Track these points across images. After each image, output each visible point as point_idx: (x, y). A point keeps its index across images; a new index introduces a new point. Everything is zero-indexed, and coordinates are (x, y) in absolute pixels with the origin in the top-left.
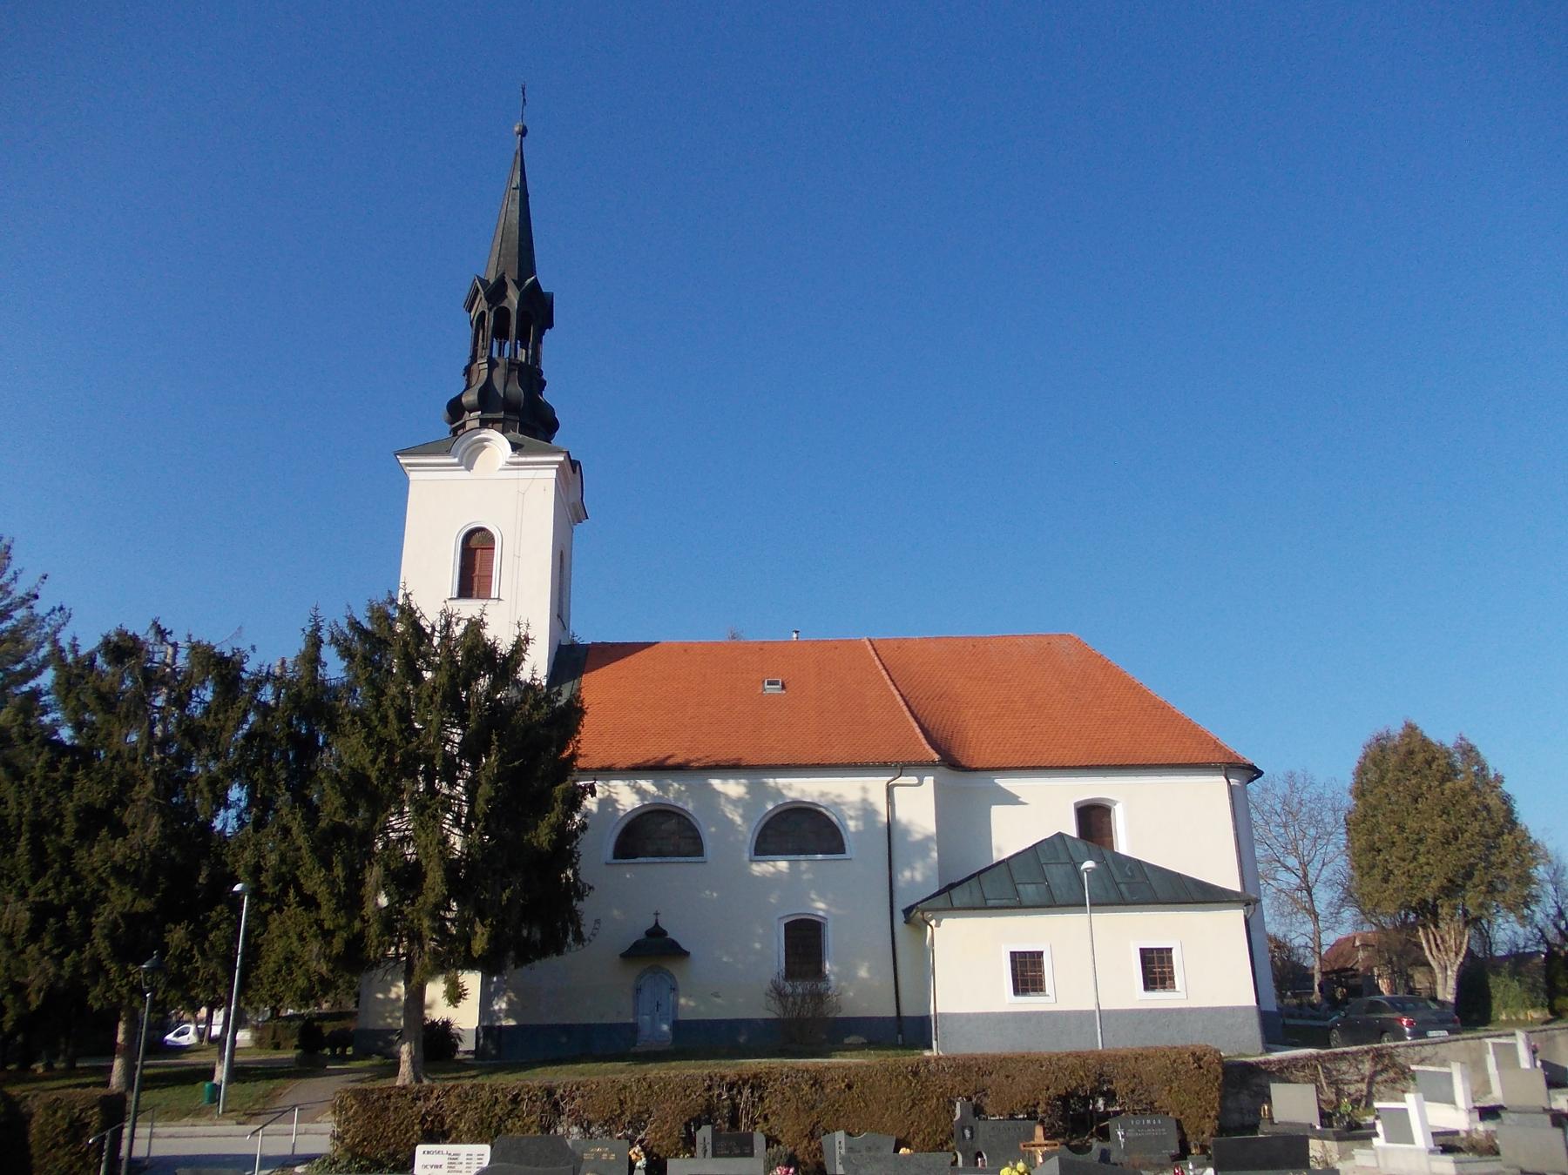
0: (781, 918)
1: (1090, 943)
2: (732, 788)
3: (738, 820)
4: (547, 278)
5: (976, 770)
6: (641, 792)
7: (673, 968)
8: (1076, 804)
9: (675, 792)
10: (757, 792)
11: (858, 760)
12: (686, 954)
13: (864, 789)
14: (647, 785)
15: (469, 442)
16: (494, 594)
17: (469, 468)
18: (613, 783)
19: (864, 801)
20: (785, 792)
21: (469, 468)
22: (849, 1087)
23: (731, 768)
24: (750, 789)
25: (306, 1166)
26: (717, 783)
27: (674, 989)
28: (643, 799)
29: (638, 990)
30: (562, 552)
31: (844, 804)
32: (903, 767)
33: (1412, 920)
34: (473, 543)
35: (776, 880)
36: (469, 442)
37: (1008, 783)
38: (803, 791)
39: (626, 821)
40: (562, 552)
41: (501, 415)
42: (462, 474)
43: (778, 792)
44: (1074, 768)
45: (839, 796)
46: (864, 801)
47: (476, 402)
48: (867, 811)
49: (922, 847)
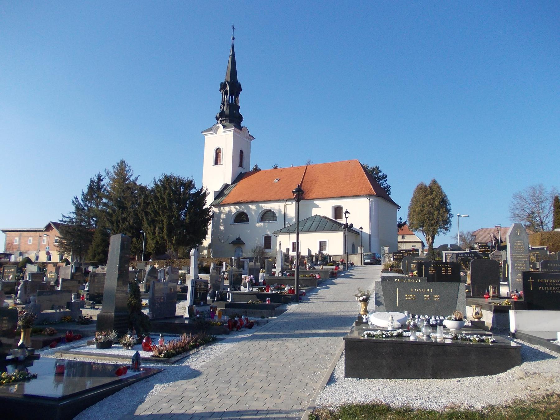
0: (263, 236)
1: (371, 244)
2: (253, 207)
3: (254, 214)
4: (240, 79)
5: (308, 200)
6: (236, 209)
7: (242, 246)
8: (333, 207)
9: (243, 208)
10: (258, 207)
11: (278, 199)
12: (245, 243)
13: (279, 206)
14: (237, 207)
15: (215, 127)
16: (221, 164)
17: (216, 133)
18: (231, 207)
19: (279, 209)
20: (263, 207)
21: (216, 133)
22: (185, 262)
23: (252, 202)
24: (257, 207)
25: (399, 316)
26: (250, 206)
27: (242, 251)
28: (236, 210)
29: (235, 251)
30: (241, 152)
31: (275, 210)
32: (287, 200)
33: (84, 223)
34: (218, 151)
35: (261, 227)
36: (215, 127)
37: (317, 202)
38: (267, 207)
39: (235, 215)
40: (241, 152)
41: (224, 119)
42: (215, 135)
43: (262, 208)
44: (332, 198)
45: (274, 208)
46: (279, 209)
47: (229, 113)
48: (280, 211)
49: (291, 219)
